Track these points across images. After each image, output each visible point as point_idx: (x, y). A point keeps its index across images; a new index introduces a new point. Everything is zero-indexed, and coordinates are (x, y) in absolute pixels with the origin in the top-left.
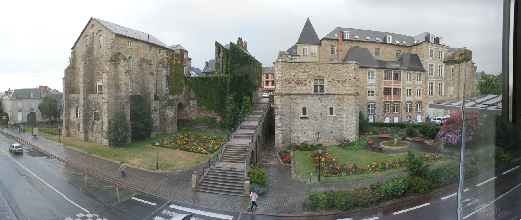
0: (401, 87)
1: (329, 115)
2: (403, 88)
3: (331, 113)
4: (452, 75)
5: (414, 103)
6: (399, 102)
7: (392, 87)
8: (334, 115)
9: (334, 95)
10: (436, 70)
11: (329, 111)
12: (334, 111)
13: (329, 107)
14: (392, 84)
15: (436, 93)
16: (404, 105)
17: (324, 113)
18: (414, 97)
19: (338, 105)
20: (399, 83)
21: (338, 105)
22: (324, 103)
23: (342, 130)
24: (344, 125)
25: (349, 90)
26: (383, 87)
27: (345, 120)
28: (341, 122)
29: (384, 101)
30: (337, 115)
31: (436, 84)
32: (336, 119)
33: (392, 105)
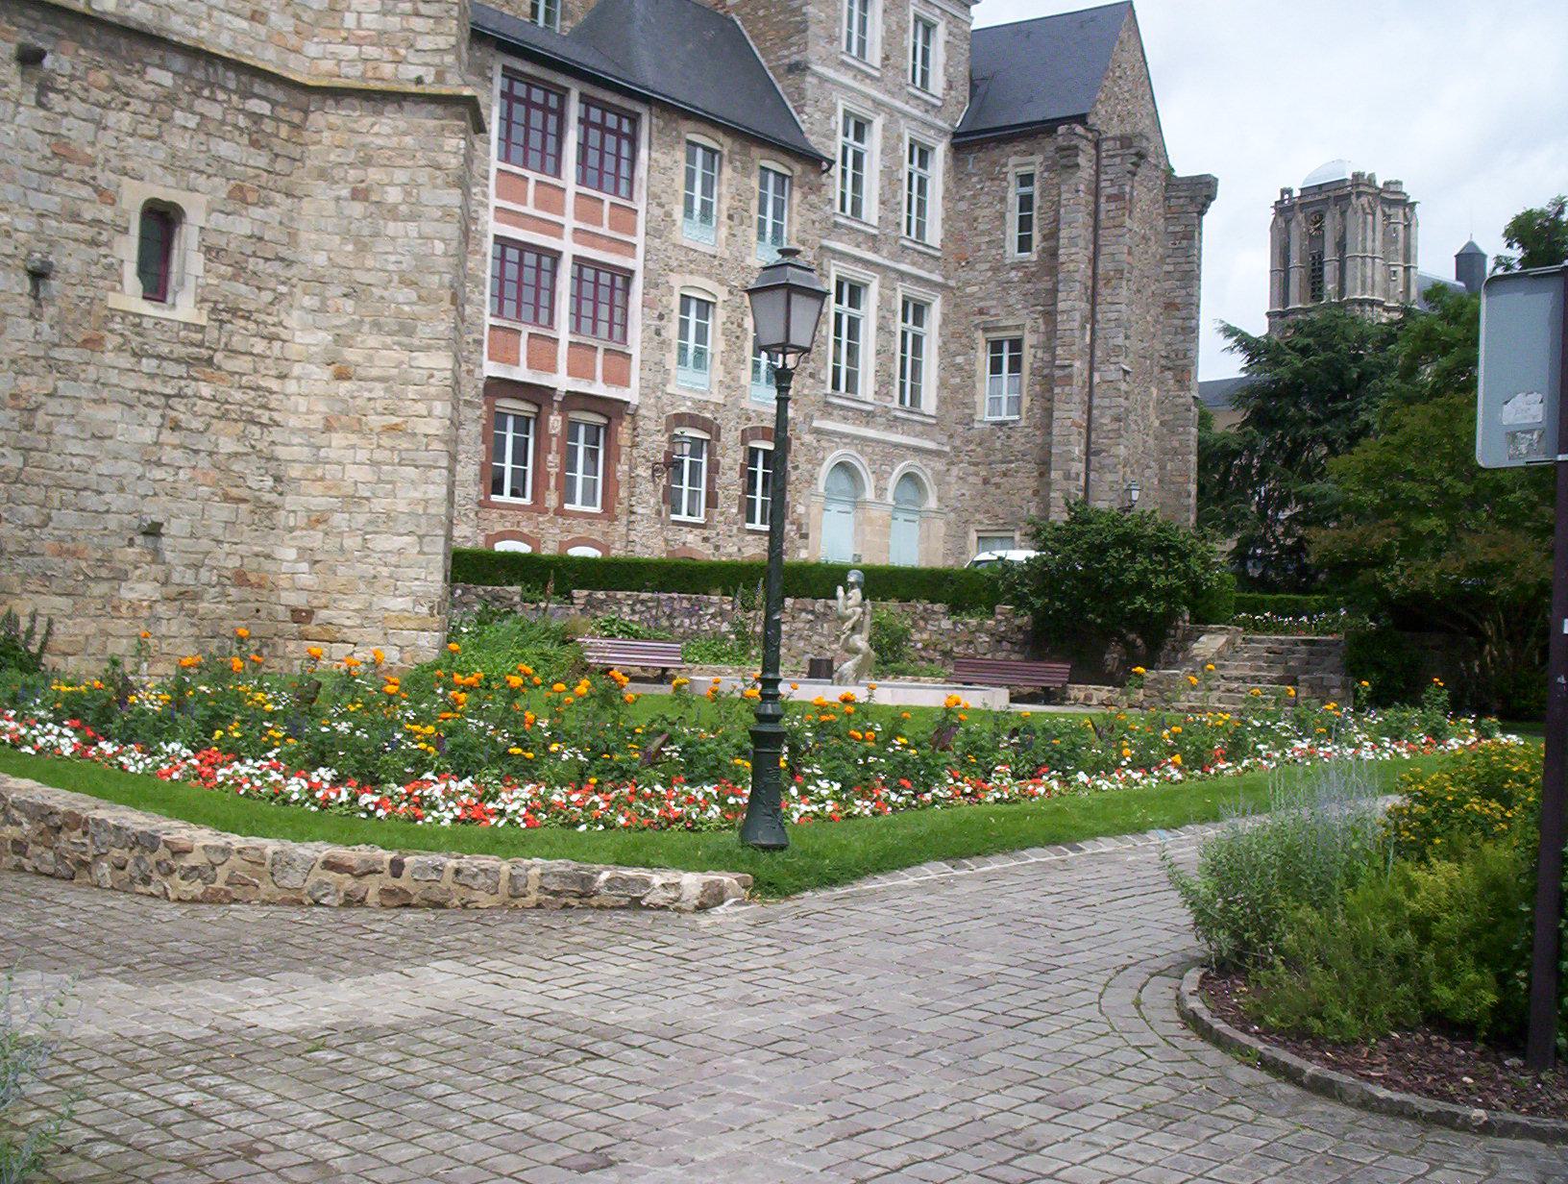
0: (636, 264)
1: (129, 296)
2: (651, 284)
3: (156, 282)
4: (1013, 233)
5: (730, 437)
6: (612, 410)
7: (568, 248)
8: (184, 308)
9: (197, 54)
10: (889, 175)
11: (128, 250)
12: (188, 259)
13: (133, 198)
14: (570, 222)
15: (883, 385)
16: (655, 443)
17: (71, 260)
18: (731, 386)
19: (239, 195)
20: (625, 217)
21: (239, 195)
22: (76, 131)
23: (266, 511)
24: (293, 452)
25: (380, 38)
26: (493, 227)
27: (305, 395)
28: (255, 416)
29: (491, 369)
30: (225, 312)
31: (884, 304)
32: (202, 363)
33: (555, 423)
